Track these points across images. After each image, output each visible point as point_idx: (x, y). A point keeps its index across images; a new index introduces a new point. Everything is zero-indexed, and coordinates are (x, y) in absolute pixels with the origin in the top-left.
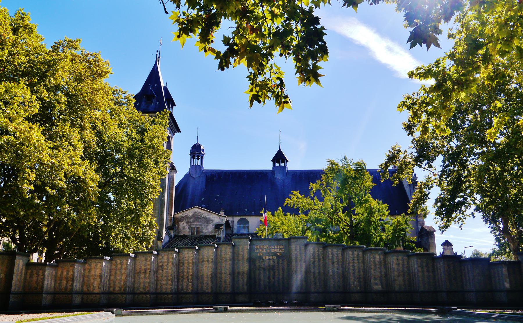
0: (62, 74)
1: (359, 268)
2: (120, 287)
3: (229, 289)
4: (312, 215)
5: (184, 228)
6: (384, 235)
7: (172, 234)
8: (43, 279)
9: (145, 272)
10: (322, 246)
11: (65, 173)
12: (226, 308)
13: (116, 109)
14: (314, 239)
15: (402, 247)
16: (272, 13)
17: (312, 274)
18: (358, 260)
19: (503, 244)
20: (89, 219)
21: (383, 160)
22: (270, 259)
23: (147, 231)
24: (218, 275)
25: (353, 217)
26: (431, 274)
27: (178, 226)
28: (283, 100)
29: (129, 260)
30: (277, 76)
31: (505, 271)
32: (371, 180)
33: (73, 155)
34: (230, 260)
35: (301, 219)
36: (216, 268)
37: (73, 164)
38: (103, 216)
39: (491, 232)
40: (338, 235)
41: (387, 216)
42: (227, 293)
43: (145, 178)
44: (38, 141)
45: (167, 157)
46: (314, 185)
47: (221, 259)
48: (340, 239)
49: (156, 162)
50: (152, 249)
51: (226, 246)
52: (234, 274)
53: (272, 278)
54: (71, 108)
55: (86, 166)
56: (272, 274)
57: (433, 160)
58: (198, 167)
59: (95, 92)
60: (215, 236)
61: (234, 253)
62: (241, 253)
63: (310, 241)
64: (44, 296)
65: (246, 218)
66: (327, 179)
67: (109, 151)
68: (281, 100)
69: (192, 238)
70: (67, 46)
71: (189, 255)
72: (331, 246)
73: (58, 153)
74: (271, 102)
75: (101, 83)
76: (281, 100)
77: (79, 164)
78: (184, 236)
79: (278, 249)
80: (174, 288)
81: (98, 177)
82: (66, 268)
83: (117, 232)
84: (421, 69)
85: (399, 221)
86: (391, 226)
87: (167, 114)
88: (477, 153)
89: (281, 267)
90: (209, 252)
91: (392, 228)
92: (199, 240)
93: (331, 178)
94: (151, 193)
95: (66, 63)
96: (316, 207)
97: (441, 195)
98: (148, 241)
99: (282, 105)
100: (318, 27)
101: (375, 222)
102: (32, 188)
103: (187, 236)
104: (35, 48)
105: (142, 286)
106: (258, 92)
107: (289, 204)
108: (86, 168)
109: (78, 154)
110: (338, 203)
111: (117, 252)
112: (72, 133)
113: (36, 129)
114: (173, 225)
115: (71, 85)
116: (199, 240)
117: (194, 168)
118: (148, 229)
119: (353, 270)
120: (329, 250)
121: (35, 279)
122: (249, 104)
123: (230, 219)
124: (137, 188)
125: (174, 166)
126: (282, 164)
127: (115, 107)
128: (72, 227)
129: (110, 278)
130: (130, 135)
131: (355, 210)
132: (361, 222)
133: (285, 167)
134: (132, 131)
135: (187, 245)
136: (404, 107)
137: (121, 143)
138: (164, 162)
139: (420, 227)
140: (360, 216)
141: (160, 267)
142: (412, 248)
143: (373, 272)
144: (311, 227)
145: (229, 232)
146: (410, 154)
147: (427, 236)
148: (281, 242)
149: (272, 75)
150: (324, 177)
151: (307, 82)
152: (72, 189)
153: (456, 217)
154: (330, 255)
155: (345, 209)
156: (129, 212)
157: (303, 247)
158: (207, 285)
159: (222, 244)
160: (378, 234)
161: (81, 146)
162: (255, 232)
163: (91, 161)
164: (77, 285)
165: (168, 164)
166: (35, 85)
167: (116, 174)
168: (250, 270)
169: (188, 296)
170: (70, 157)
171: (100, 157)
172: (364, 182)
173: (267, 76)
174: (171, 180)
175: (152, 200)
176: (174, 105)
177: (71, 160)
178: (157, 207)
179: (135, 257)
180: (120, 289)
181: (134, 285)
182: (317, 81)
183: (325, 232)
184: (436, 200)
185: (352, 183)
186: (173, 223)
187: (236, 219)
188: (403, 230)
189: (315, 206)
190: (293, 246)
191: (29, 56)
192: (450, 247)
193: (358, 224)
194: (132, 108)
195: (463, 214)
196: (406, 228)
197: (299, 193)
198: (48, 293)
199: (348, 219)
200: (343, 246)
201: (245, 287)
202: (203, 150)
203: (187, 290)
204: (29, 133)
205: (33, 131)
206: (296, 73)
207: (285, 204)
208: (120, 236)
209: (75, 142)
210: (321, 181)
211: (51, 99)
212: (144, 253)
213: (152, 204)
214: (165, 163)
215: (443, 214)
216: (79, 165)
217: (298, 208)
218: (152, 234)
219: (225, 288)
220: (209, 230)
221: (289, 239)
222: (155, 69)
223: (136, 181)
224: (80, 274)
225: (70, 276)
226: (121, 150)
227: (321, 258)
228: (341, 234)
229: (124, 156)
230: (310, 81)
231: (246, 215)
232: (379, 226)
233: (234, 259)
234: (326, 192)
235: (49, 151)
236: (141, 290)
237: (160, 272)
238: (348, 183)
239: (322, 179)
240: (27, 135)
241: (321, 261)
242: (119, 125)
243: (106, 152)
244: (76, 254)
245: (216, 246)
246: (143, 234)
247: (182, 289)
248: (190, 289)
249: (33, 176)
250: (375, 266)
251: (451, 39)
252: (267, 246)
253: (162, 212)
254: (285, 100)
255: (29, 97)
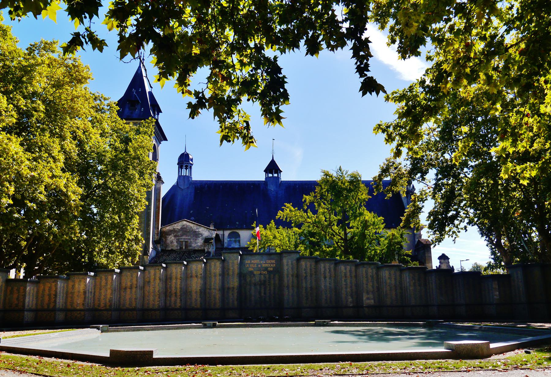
0: (40, 81)
1: (351, 283)
2: (105, 304)
3: (218, 305)
5: (172, 242)
7: (160, 249)
8: (24, 296)
9: (131, 288)
10: (314, 260)
11: (45, 186)
12: (215, 324)
13: (98, 117)
16: (241, 62)
17: (304, 289)
18: (350, 275)
19: (498, 257)
20: (71, 234)
21: (376, 172)
22: (261, 274)
23: (132, 245)
24: (208, 291)
25: (348, 230)
29: (115, 276)
30: (244, 119)
31: (495, 285)
32: (367, 192)
33: (54, 167)
34: (220, 275)
35: (294, 232)
36: (205, 283)
37: (53, 177)
38: (86, 230)
39: (487, 245)
40: (332, 249)
41: (383, 229)
43: (130, 191)
44: (16, 153)
45: (153, 169)
46: (307, 197)
47: (210, 274)
48: (333, 254)
49: (141, 174)
50: (139, 264)
52: (224, 289)
54: (50, 117)
55: (67, 178)
59: (75, 99)
61: (223, 268)
64: (26, 313)
65: (237, 231)
66: (320, 191)
67: (91, 161)
68: (248, 140)
70: (42, 49)
71: (177, 270)
72: (324, 260)
73: (38, 165)
75: (80, 89)
76: (248, 140)
77: (60, 176)
79: (269, 264)
81: (81, 190)
82: (47, 285)
83: (101, 247)
84: (396, 93)
87: (152, 122)
88: (472, 166)
89: (272, 282)
90: (198, 267)
91: (387, 241)
92: (188, 254)
94: (136, 206)
95: (44, 68)
96: (309, 220)
97: (435, 208)
98: (134, 255)
99: (248, 144)
100: (281, 76)
101: (369, 236)
102: (11, 202)
103: (175, 250)
104: (10, 53)
105: (128, 302)
107: (282, 217)
108: (68, 181)
109: (59, 165)
110: (332, 216)
111: (102, 268)
112: (52, 144)
113: (14, 140)
115: (49, 91)
116: (188, 254)
118: (133, 243)
121: (15, 296)
122: (220, 143)
123: (220, 233)
124: (122, 202)
126: (276, 175)
127: (94, 114)
128: (53, 242)
129: (94, 294)
130: (113, 145)
131: (349, 223)
133: (278, 178)
134: (115, 141)
135: (175, 259)
136: (379, 130)
137: (103, 154)
138: (150, 173)
139: (417, 240)
140: (355, 229)
141: (146, 282)
142: (407, 262)
143: (365, 286)
146: (405, 166)
148: (272, 256)
149: (240, 118)
150: (318, 189)
151: (271, 123)
152: (53, 202)
153: (450, 231)
154: (323, 270)
155: (339, 222)
156: (113, 226)
158: (196, 300)
159: (211, 259)
160: (373, 248)
161: (62, 157)
163: (73, 172)
164: (60, 302)
165: (154, 176)
166: (12, 92)
167: (98, 186)
168: (240, 286)
170: (51, 169)
171: (81, 168)
172: (359, 194)
173: (236, 118)
174: (158, 191)
175: (137, 213)
176: (159, 111)
177: (53, 174)
178: (143, 220)
179: (120, 273)
180: (105, 306)
181: (119, 302)
182: (279, 121)
184: (429, 213)
187: (227, 233)
188: (399, 243)
189: (308, 219)
190: (285, 261)
191: (4, 61)
192: (446, 261)
193: (353, 237)
194: (115, 116)
195: (457, 227)
196: (402, 242)
197: (292, 206)
198: (30, 310)
200: (337, 260)
201: (236, 303)
202: (192, 160)
204: (6, 144)
205: (11, 143)
206: (262, 115)
208: (104, 251)
209: (55, 153)
210: (315, 193)
211: (28, 107)
212: (129, 268)
213: (138, 217)
214: (150, 174)
216: (60, 177)
217: (290, 221)
218: (138, 248)
222: (139, 72)
223: (120, 193)
224: (63, 290)
225: (53, 292)
226: (103, 161)
228: (335, 248)
229: (107, 167)
230: (273, 122)
232: (374, 239)
233: (224, 273)
234: (319, 205)
235: (27, 162)
236: (127, 306)
237: (147, 288)
239: (316, 191)
240: (5, 146)
241: (314, 276)
242: (101, 134)
243: (88, 163)
244: (57, 269)
245: (205, 260)
246: (129, 249)
248: (178, 305)
249: (12, 189)
250: (367, 280)
251: (429, 61)
253: (149, 225)
254: (251, 140)
255: (6, 106)
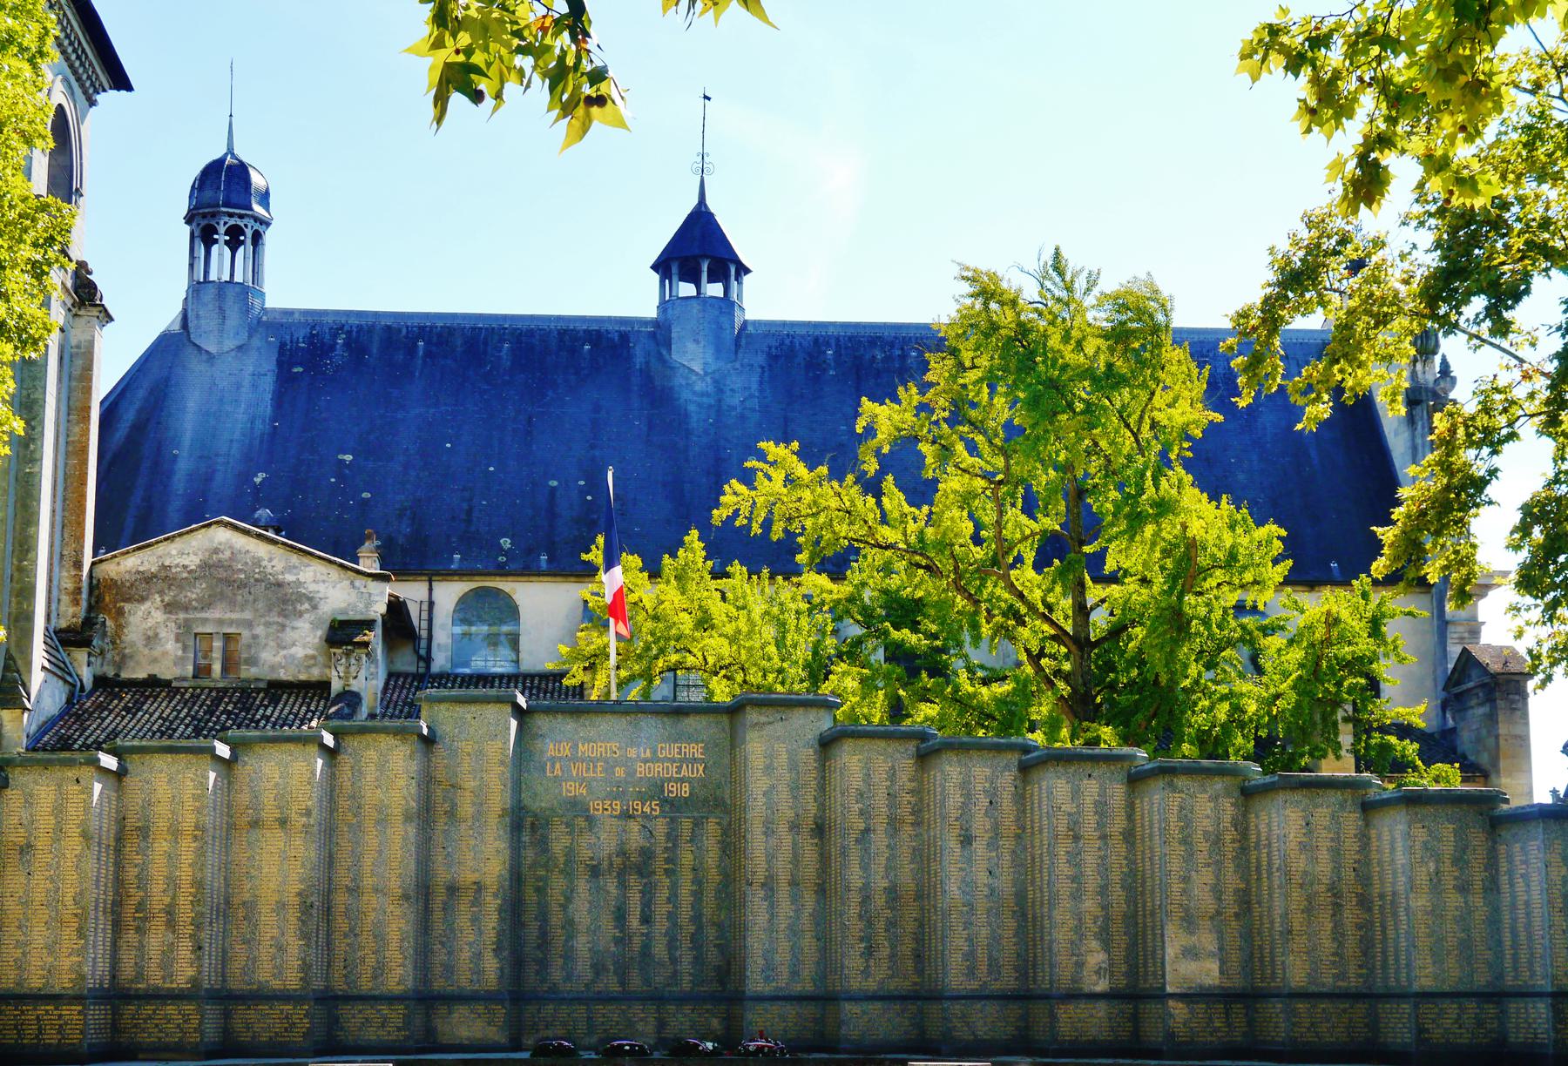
1: (1103, 868)
3: (399, 976)
4: (866, 579)
5: (151, 639)
6: (1252, 696)
7: (86, 675)
10: (911, 747)
14: (876, 711)
15: (1350, 760)
17: (855, 898)
22: (626, 816)
24: (341, 899)
25: (1094, 593)
26: (1477, 901)
27: (120, 627)
28: (587, 90)
34: (408, 818)
35: (808, 598)
40: (1008, 687)
42: (391, 999)
45: (51, 240)
48: (1010, 716)
51: (386, 741)
53: (634, 922)
56: (635, 899)
57: (1517, 297)
58: (231, 293)
60: (324, 685)
61: (427, 781)
62: (471, 784)
63: (852, 716)
65: (506, 585)
66: (954, 377)
69: (195, 697)
71: (178, 787)
74: (528, 100)
78: (153, 684)
79: (666, 758)
80: (95, 970)
85: (1337, 621)
86: (1291, 642)
89: (686, 858)
90: (287, 773)
91: (1297, 654)
92: (235, 706)
93: (973, 375)
96: (888, 534)
101: (1206, 622)
103: (168, 683)
106: (469, 52)
107: (745, 511)
110: (1014, 515)
114: (89, 622)
116: (235, 706)
117: (209, 294)
119: (1074, 879)
120: (950, 771)
122: (430, 111)
123: (412, 592)
125: (92, 287)
126: (715, 290)
131: (1101, 556)
132: (1133, 623)
133: (727, 305)
138: (34, 264)
139: (1454, 650)
140: (1131, 584)
142: (1400, 766)
143: (1176, 887)
144: (859, 642)
145: (406, 662)
146: (1403, 257)
147: (1491, 700)
148: (691, 723)
150: (939, 369)
154: (955, 799)
155: (1050, 550)
157: (808, 755)
159: (363, 731)
160: (1223, 689)
162: (550, 666)
168: (516, 877)
169: (171, 1009)
172: (1158, 401)
174: (78, 364)
183: (939, 671)
184: (1526, 509)
185: (1089, 408)
186: (90, 608)
187: (448, 594)
188: (1358, 665)
193: (1117, 631)
197: (802, 455)
199: (1067, 603)
200: (1026, 749)
202: (265, 198)
203: (169, 976)
207: (719, 515)
210: (924, 387)
214: (38, 271)
215: (1554, 587)
219: (380, 970)
220: (292, 650)
221: (734, 710)
227: (904, 812)
228: (1022, 688)
231: (502, 572)
232: (1230, 643)
233: (431, 810)
238: (1070, 406)
239: (930, 377)
247: (139, 976)
252: (614, 745)
